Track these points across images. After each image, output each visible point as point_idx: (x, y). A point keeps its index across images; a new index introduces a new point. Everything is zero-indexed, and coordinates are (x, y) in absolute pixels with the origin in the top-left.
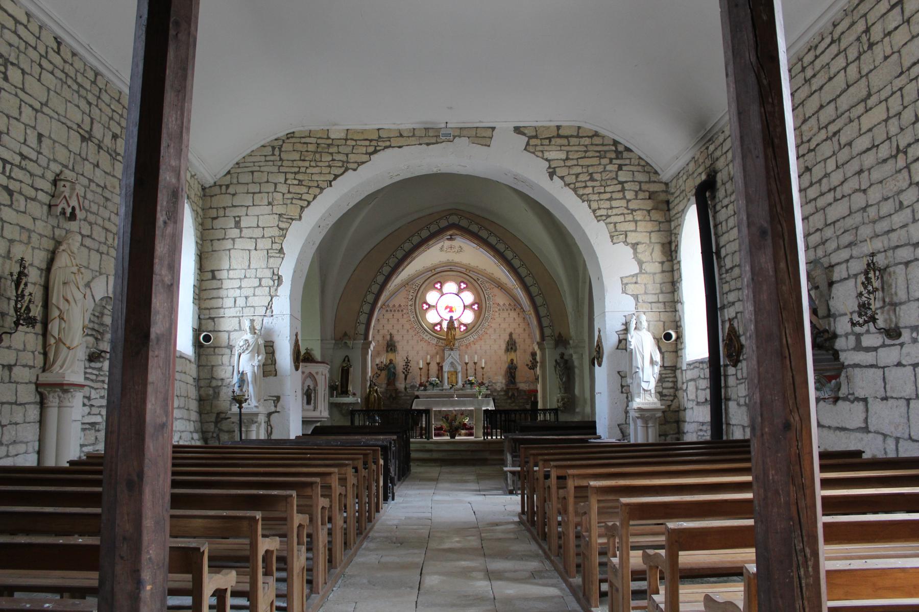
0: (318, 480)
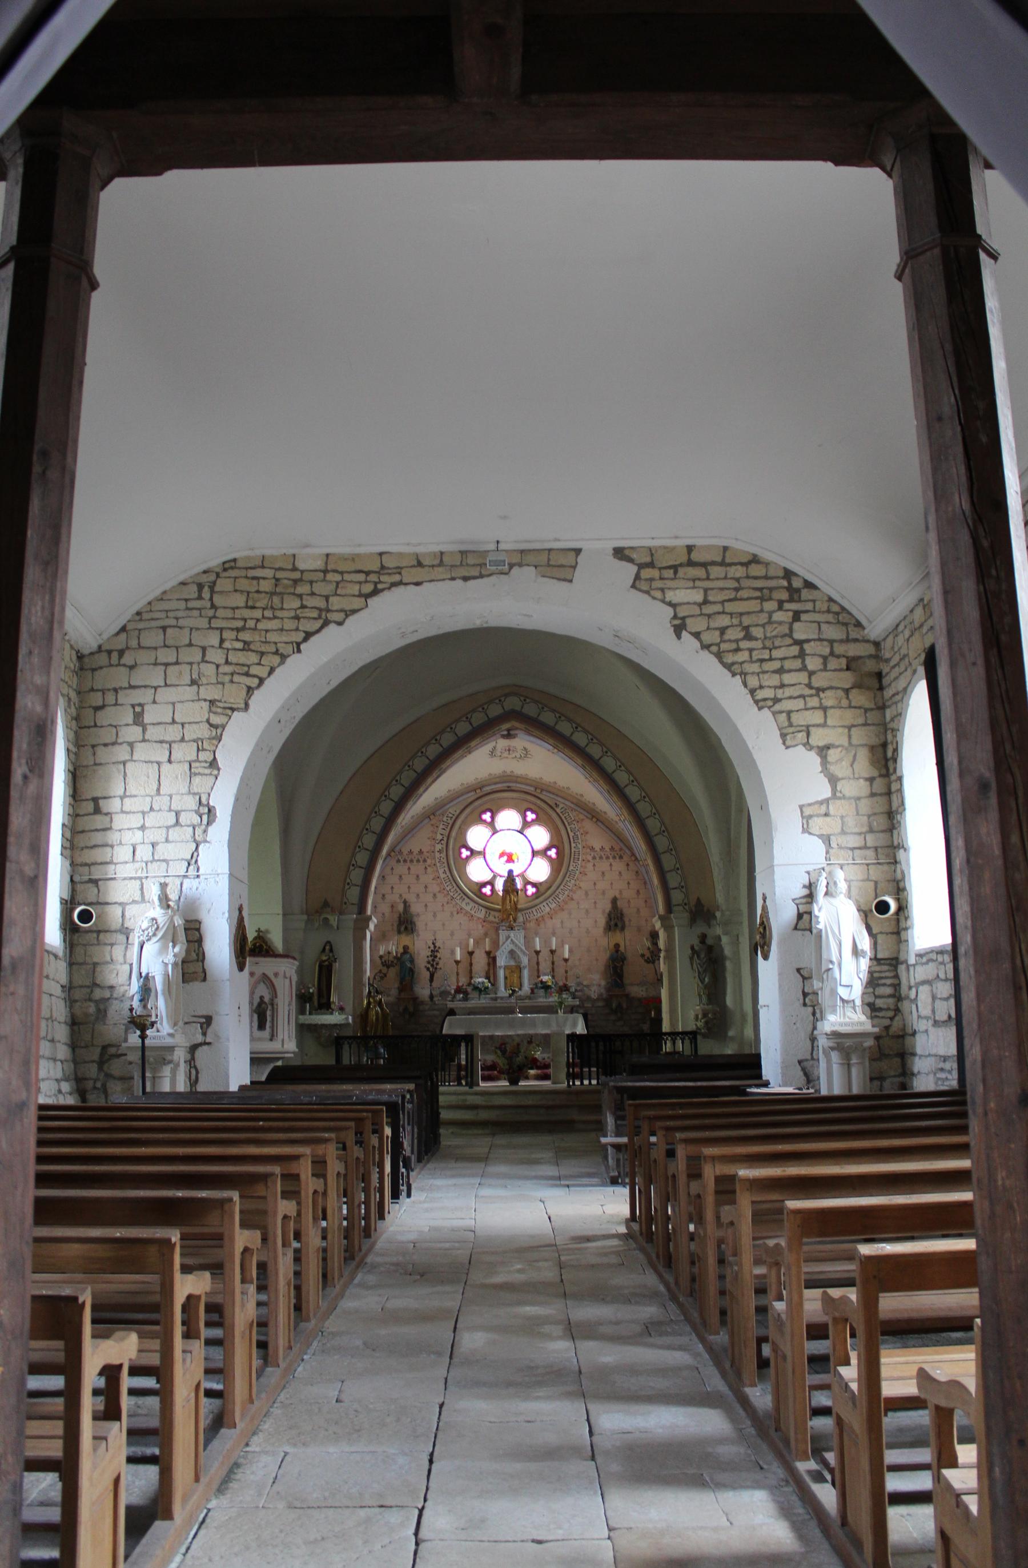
0: (277, 1169)
